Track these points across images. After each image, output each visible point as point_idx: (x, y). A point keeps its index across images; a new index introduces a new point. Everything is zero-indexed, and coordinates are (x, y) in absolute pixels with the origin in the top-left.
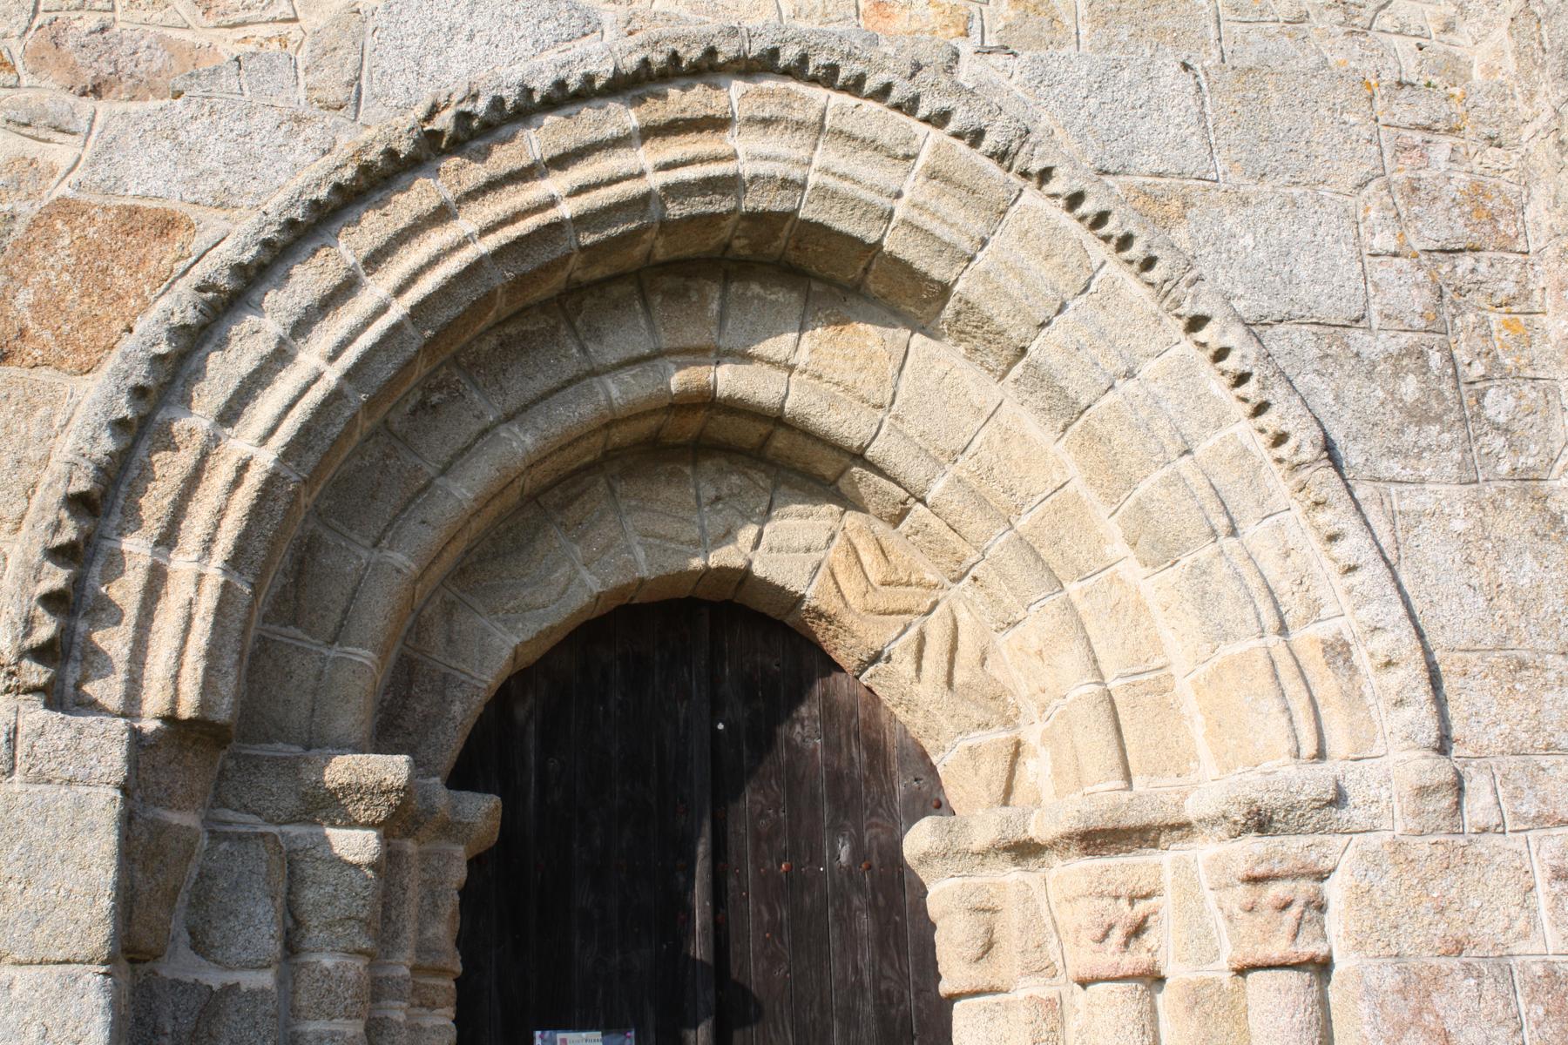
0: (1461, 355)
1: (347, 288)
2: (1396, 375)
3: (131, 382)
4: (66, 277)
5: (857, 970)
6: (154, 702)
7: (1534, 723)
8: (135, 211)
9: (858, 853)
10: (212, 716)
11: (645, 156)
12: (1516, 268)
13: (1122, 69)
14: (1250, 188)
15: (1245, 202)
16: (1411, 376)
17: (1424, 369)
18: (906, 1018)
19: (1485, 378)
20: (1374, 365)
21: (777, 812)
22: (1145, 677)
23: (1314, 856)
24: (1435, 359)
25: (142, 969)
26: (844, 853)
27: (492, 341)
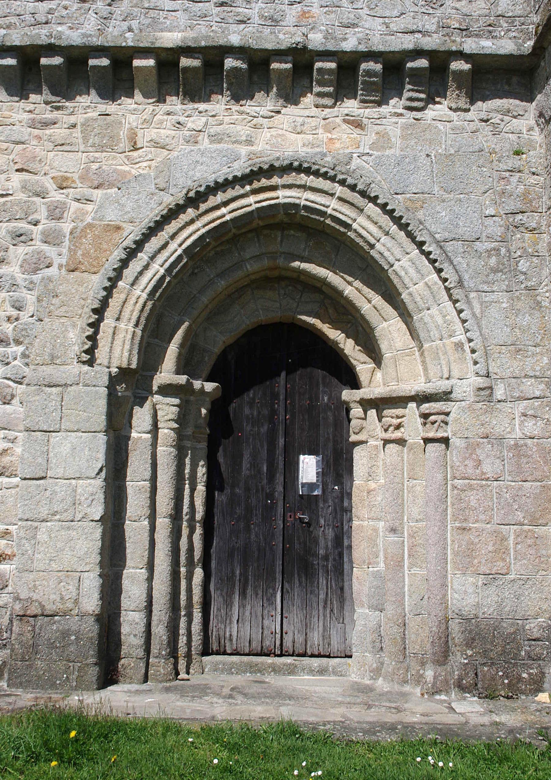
0: (513, 249)
1: (164, 246)
2: (489, 257)
3: (107, 276)
4: (90, 246)
5: (328, 434)
6: (115, 363)
7: (522, 368)
8: (108, 225)
9: (329, 399)
10: (131, 367)
11: (252, 199)
12: (537, 218)
13: (406, 158)
14: (446, 196)
15: (444, 201)
16: (494, 257)
17: (498, 255)
18: (342, 449)
19: (520, 256)
20: (481, 253)
21: (306, 386)
22: (406, 351)
23: (444, 408)
24: (503, 250)
25: (117, 432)
26: (326, 398)
27: (213, 252)
